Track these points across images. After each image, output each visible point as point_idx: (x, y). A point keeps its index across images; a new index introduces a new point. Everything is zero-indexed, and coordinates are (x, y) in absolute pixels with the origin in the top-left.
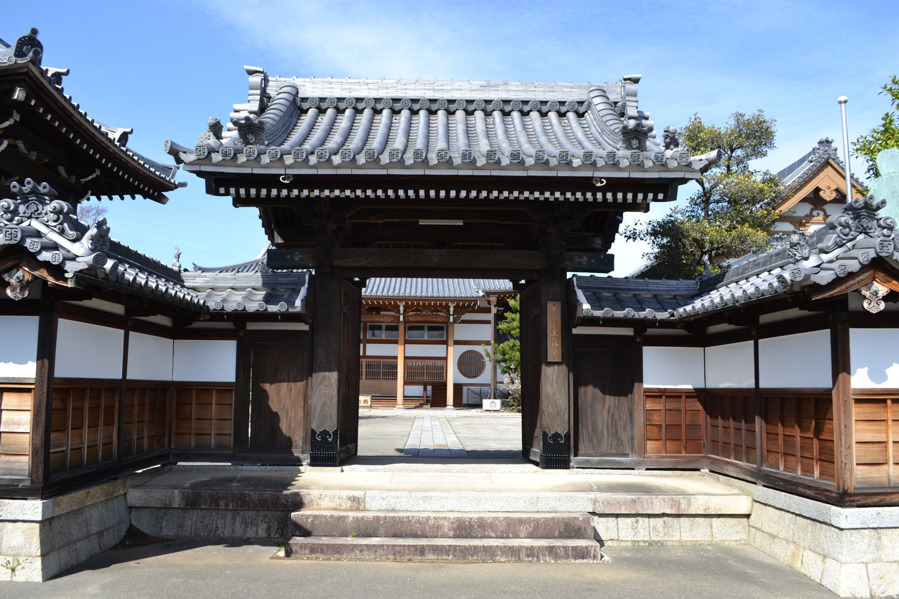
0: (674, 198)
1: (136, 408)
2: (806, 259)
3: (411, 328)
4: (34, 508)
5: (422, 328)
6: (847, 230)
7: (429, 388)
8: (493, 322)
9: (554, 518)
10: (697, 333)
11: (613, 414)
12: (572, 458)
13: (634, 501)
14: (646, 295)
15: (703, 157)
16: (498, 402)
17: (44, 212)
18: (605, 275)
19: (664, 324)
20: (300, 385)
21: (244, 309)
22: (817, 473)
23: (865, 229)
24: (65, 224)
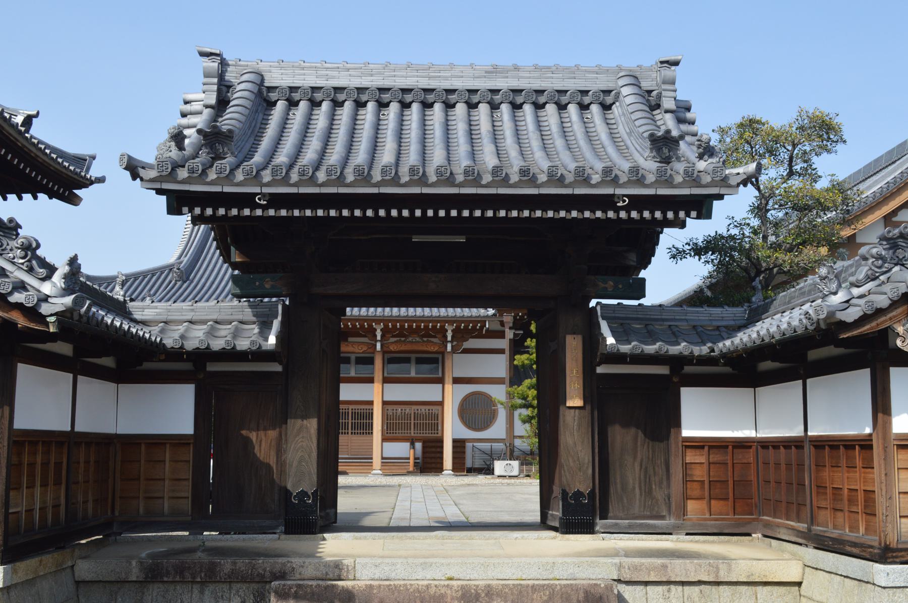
0: (708, 216)
1: (82, 465)
2: (835, 293)
3: (391, 361)
5: (407, 361)
6: (880, 262)
7: (419, 446)
8: (507, 352)
9: (572, 585)
10: (747, 371)
11: (646, 468)
12: (598, 521)
13: (665, 567)
14: (683, 325)
15: (741, 170)
16: (515, 464)
17: (9, 247)
18: (635, 303)
19: (703, 360)
20: (272, 434)
21: (208, 348)
22: (862, 530)
23: (901, 260)
24: (34, 262)
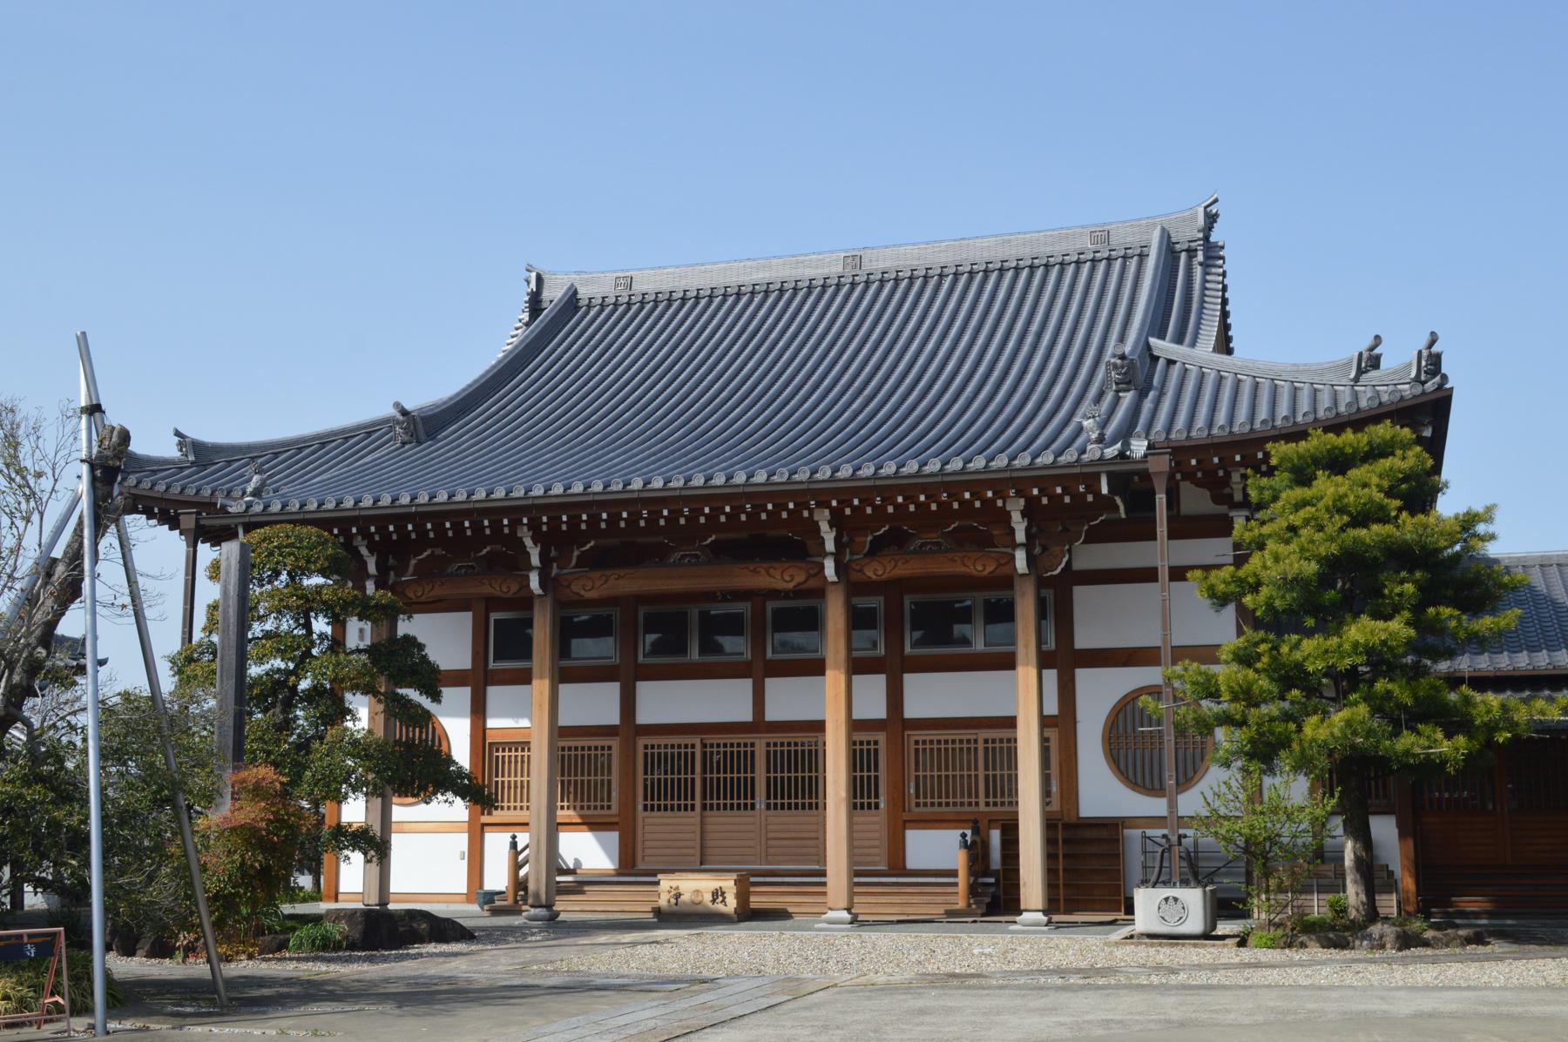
16: (1193, 898)
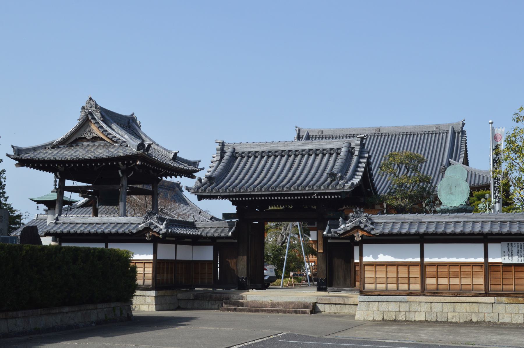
4: (153, 293)
13: (330, 299)
20: (235, 260)
